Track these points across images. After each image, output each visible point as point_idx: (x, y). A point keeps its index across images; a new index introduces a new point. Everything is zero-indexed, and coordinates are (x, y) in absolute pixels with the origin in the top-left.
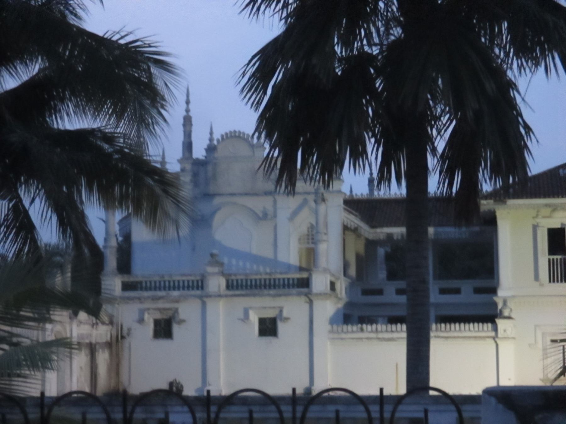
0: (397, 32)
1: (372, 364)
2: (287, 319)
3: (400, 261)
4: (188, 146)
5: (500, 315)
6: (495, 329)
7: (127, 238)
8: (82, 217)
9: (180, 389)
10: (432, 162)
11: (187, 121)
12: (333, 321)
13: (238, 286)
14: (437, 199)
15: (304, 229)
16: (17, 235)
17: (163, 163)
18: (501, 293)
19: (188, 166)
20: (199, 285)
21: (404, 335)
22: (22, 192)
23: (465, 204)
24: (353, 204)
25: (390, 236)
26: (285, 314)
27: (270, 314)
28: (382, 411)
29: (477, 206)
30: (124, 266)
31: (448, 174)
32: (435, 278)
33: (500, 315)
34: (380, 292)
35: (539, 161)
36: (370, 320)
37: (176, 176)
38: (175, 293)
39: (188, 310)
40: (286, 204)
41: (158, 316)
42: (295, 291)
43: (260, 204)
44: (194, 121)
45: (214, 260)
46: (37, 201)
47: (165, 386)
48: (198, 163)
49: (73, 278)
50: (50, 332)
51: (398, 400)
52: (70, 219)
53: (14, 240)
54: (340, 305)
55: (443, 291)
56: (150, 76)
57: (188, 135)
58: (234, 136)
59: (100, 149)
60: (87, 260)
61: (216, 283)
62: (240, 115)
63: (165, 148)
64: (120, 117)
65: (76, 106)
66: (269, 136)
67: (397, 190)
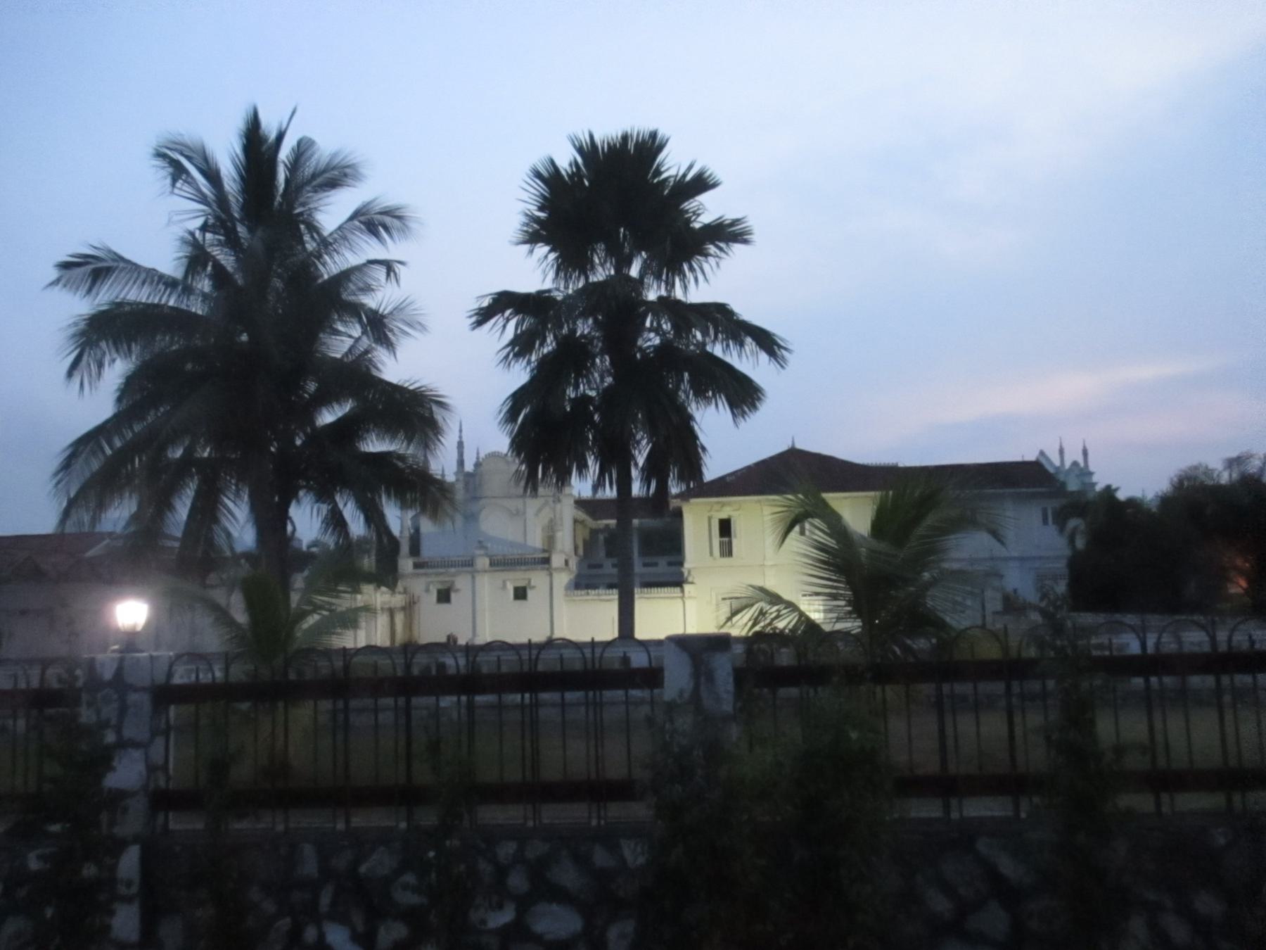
0: (609, 380)
1: (590, 620)
2: (534, 587)
3: (615, 544)
4: (461, 463)
5: (686, 581)
6: (683, 591)
7: (417, 530)
8: (382, 516)
9: (455, 641)
10: (635, 473)
11: (460, 445)
12: (567, 588)
13: (501, 564)
14: (639, 499)
15: (546, 521)
16: (334, 529)
17: (443, 475)
18: (687, 565)
19: (461, 478)
20: (469, 564)
21: (616, 597)
22: (338, 498)
23: (658, 503)
24: (581, 503)
25: (607, 526)
26: (533, 583)
27: (521, 584)
28: (593, 652)
29: (667, 504)
30: (415, 549)
31: (646, 480)
32: (643, 553)
33: (686, 581)
34: (600, 566)
35: (713, 469)
36: (595, 587)
37: (452, 485)
38: (453, 570)
39: (462, 582)
40: (532, 505)
41: (440, 587)
42: (540, 566)
43: (519, 503)
44: (465, 444)
45: (481, 545)
46: (349, 505)
47: (443, 640)
48: (469, 475)
49: (378, 561)
50: (360, 600)
51: (607, 645)
52: (374, 517)
53: (333, 533)
54: (572, 576)
55: (645, 565)
56: (431, 412)
57: (461, 454)
58: (494, 455)
59: (395, 465)
60: (387, 549)
61: (483, 562)
62: (500, 441)
63: (443, 463)
64: (410, 441)
65: (378, 435)
66: (518, 455)
67: (610, 493)
